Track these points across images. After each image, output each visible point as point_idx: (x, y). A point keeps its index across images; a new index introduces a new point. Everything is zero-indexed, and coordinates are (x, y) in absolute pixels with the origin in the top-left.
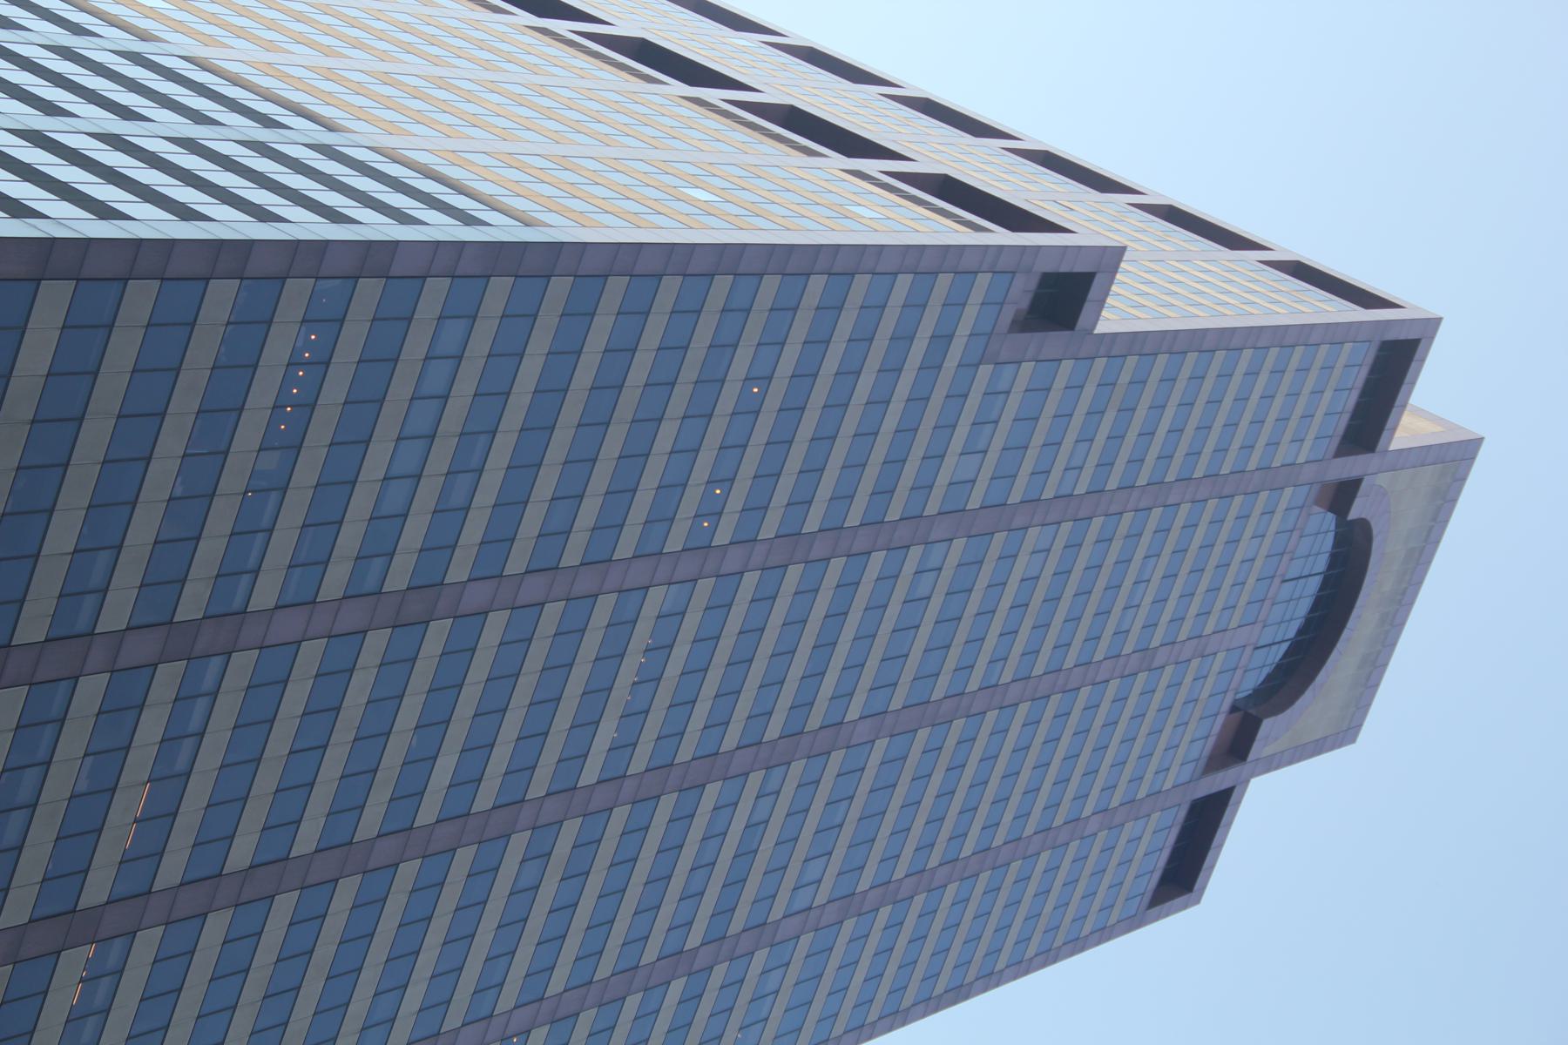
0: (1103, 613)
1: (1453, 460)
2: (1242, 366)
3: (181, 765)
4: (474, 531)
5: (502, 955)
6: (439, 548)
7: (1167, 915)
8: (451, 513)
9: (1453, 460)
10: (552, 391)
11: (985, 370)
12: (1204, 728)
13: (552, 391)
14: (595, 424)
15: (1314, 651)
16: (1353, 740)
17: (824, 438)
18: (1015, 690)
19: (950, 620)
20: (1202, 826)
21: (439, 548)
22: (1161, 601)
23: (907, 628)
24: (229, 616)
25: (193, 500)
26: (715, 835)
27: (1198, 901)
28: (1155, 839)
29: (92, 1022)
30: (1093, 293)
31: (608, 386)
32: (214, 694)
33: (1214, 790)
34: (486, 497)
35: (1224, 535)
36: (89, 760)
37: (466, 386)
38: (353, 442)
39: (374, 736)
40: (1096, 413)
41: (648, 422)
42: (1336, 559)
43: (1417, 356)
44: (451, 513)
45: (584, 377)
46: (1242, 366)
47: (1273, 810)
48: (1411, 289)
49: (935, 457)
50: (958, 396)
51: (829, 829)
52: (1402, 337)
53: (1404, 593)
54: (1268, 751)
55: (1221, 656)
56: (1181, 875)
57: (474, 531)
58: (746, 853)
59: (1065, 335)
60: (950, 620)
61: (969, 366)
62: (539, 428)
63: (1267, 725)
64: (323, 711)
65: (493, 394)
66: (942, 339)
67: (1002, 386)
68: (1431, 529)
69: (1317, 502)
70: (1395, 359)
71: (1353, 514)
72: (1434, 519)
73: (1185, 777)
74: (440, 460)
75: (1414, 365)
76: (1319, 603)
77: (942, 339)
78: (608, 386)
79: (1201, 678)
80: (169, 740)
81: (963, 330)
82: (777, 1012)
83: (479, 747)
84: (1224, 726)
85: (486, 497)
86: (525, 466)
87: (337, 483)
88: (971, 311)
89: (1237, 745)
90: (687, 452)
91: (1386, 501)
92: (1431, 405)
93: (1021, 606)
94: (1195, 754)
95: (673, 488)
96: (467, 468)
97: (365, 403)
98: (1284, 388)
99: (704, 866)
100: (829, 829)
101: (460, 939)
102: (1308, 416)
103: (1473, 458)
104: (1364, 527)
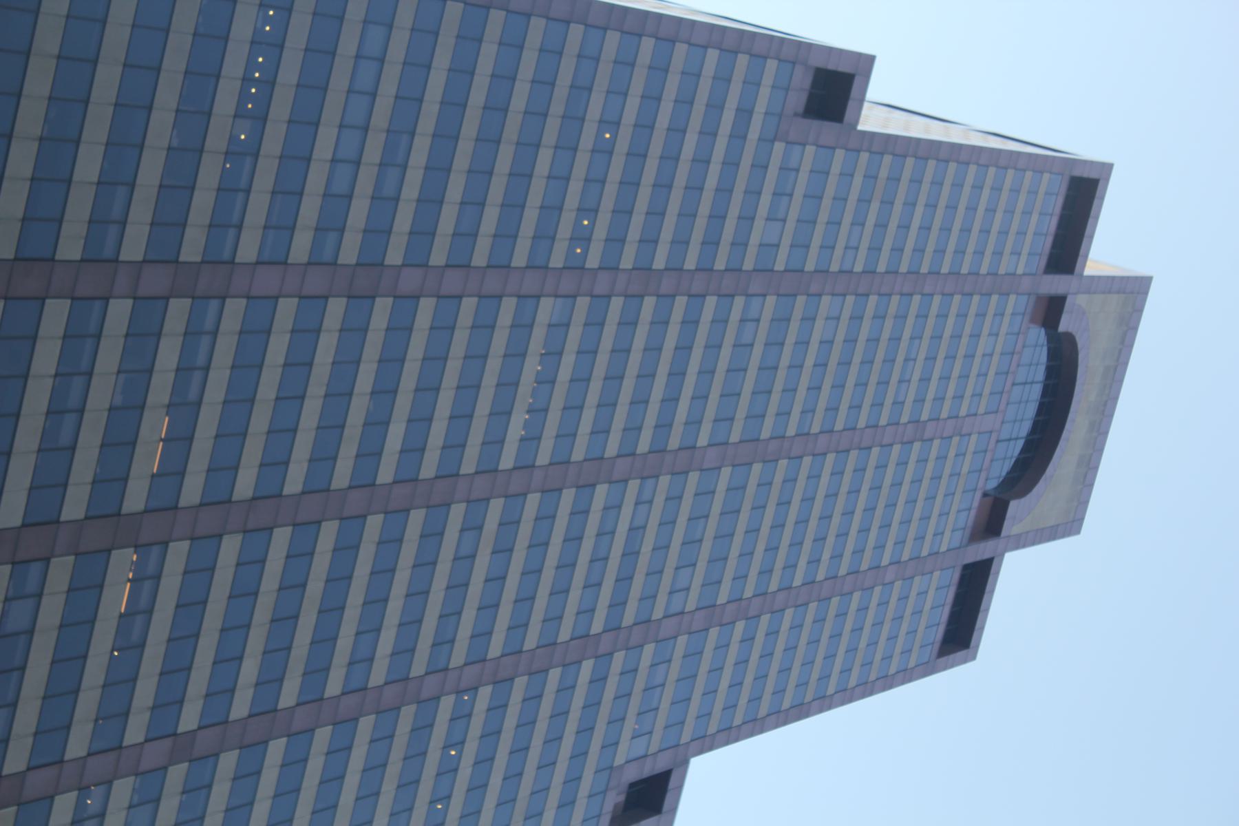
0: (884, 383)
1: (1131, 292)
2: (854, 606)
3: (192, 395)
4: (404, 220)
5: (451, 614)
6: (378, 232)
7: (952, 666)
8: (385, 202)
9: (1131, 292)
10: (454, 104)
11: (779, 147)
12: (962, 509)
13: (454, 104)
14: (489, 140)
15: (1040, 449)
16: (1078, 532)
17: (663, 186)
18: (781, 597)
19: (769, 369)
20: (973, 586)
21: (378, 232)
22: (925, 380)
23: (736, 370)
24: (219, 261)
25: (185, 155)
26: (606, 533)
27: (974, 658)
28: (936, 596)
29: (139, 619)
30: (672, 783)
31: (497, 108)
32: (207, 369)
33: (979, 558)
34: (410, 192)
35: (890, 615)
36: (122, 376)
37: (388, 88)
38: (305, 122)
39: (339, 395)
40: (864, 201)
41: (529, 146)
42: (1051, 372)
43: (992, 571)
44: (385, 202)
45: (477, 98)
46: (854, 606)
47: (1024, 577)
48: (1080, 143)
49: (747, 219)
50: (761, 167)
51: (692, 542)
52: (1085, 175)
53: (1105, 405)
54: (1015, 530)
55: (974, 438)
56: (959, 634)
57: (404, 220)
58: (631, 554)
59: (834, 126)
60: (769, 369)
61: (767, 141)
62: (446, 136)
63: (1014, 507)
64: (244, 593)
65: (409, 100)
66: (745, 113)
67: (659, 680)
68: (1120, 351)
69: (1032, 321)
70: (1081, 192)
71: (1062, 328)
72: (1122, 342)
73: (956, 544)
74: (373, 153)
75: (1091, 221)
76: (1043, 409)
77: (745, 113)
78: (497, 108)
79: (960, 455)
80: (183, 370)
81: (760, 108)
82: (665, 705)
83: (420, 421)
84: (980, 505)
85: (410, 192)
86: (439, 169)
87: (297, 158)
88: (765, 92)
89: (991, 522)
90: (560, 179)
91: (1085, 320)
92: (1105, 253)
93: (821, 365)
94: (961, 524)
95: (552, 210)
96: (393, 161)
97: (313, 87)
98: (917, 514)
99: (599, 559)
100: (692, 542)
101: (417, 594)
102: (918, 612)
103: (1146, 293)
104: (1070, 339)
